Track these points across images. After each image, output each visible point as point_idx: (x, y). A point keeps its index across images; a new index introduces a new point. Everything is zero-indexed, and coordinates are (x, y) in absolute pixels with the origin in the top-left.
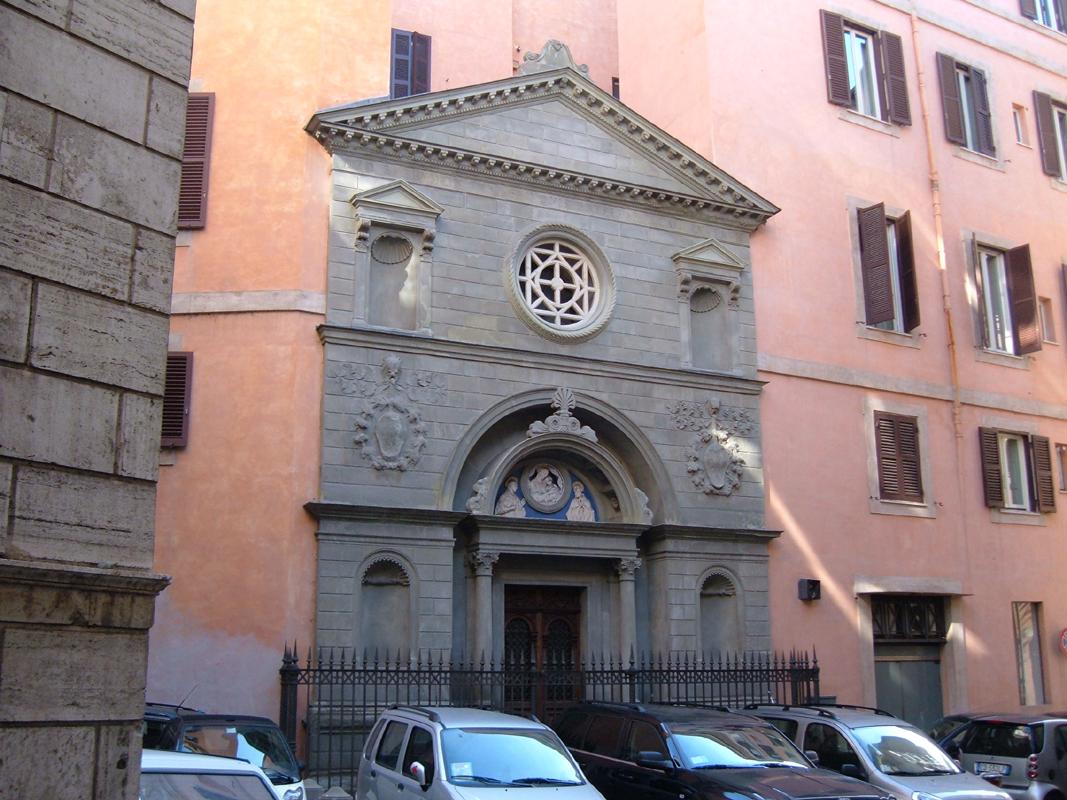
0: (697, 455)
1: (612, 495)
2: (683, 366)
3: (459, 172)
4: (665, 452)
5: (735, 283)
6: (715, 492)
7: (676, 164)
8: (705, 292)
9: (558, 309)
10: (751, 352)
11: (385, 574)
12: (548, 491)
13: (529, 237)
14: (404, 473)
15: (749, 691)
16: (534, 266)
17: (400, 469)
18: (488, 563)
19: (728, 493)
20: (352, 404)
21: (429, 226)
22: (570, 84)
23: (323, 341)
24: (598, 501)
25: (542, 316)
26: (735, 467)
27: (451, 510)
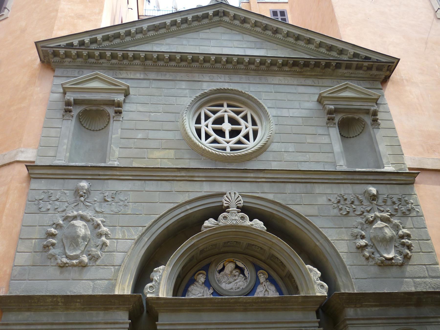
2: (338, 169)
3: (145, 69)
6: (387, 264)
7: (312, 46)
9: (228, 142)
12: (235, 280)
13: (198, 99)
14: (85, 269)
17: (82, 266)
20: (47, 219)
23: (31, 177)
27: (165, 296)
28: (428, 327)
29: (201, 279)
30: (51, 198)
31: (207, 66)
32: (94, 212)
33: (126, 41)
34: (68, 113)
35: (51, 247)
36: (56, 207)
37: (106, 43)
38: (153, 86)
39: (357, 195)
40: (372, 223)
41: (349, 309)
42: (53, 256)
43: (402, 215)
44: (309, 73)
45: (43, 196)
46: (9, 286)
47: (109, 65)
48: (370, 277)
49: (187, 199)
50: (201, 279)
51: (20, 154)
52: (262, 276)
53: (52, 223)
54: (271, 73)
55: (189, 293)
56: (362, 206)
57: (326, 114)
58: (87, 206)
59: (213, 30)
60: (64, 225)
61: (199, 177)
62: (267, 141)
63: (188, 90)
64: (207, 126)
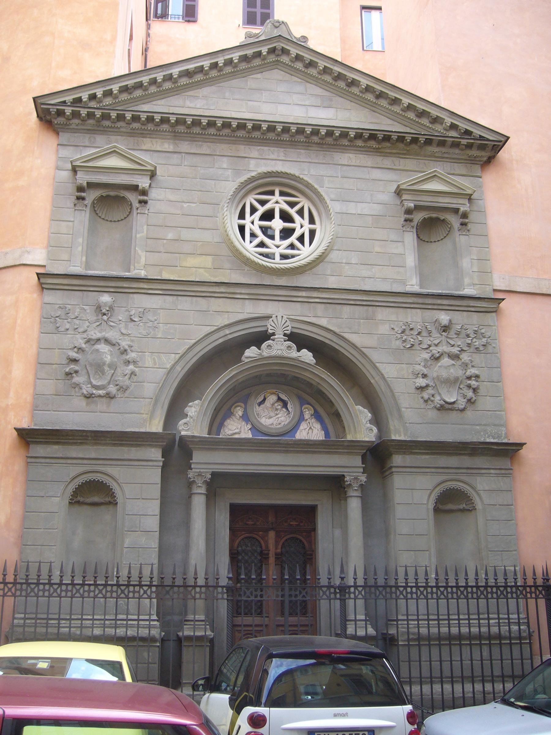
0: (425, 371)
1: (337, 416)
2: (409, 289)
3: (176, 136)
4: (390, 370)
5: (462, 209)
6: (446, 408)
7: (397, 109)
8: (432, 222)
9: (278, 247)
10: (485, 273)
11: (93, 495)
12: (277, 415)
14: (113, 401)
15: (493, 608)
16: (253, 210)
17: (110, 397)
18: (199, 482)
19: (463, 407)
20: (67, 340)
21: (143, 182)
22: (285, 51)
23: (42, 287)
24: (327, 420)
25: (261, 254)
26: (469, 382)
28: (478, 478)
29: (239, 412)
30: (69, 315)
31: (256, 136)
32: (120, 333)
33: (150, 92)
34: (81, 201)
35: (74, 375)
36: (76, 327)
37: (124, 96)
38: (186, 164)
39: (426, 324)
40: (437, 359)
41: (397, 456)
42: (77, 386)
43: (475, 351)
44: (388, 151)
45: (59, 313)
46: (33, 416)
47: (129, 131)
48: (425, 422)
49: (227, 322)
50: (239, 412)
51: (26, 255)
52: (307, 412)
53: (73, 346)
54: (339, 149)
55: (225, 428)
56: (429, 338)
57: (403, 213)
58: (111, 326)
59: (266, 74)
60: (87, 349)
61: (241, 294)
62: (326, 250)
63: (230, 171)
64: (253, 223)
